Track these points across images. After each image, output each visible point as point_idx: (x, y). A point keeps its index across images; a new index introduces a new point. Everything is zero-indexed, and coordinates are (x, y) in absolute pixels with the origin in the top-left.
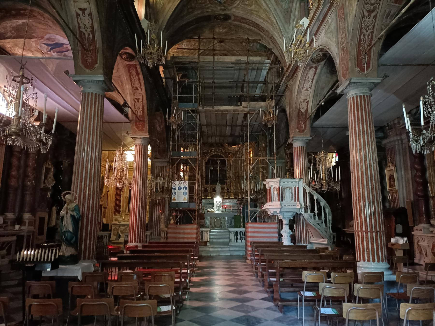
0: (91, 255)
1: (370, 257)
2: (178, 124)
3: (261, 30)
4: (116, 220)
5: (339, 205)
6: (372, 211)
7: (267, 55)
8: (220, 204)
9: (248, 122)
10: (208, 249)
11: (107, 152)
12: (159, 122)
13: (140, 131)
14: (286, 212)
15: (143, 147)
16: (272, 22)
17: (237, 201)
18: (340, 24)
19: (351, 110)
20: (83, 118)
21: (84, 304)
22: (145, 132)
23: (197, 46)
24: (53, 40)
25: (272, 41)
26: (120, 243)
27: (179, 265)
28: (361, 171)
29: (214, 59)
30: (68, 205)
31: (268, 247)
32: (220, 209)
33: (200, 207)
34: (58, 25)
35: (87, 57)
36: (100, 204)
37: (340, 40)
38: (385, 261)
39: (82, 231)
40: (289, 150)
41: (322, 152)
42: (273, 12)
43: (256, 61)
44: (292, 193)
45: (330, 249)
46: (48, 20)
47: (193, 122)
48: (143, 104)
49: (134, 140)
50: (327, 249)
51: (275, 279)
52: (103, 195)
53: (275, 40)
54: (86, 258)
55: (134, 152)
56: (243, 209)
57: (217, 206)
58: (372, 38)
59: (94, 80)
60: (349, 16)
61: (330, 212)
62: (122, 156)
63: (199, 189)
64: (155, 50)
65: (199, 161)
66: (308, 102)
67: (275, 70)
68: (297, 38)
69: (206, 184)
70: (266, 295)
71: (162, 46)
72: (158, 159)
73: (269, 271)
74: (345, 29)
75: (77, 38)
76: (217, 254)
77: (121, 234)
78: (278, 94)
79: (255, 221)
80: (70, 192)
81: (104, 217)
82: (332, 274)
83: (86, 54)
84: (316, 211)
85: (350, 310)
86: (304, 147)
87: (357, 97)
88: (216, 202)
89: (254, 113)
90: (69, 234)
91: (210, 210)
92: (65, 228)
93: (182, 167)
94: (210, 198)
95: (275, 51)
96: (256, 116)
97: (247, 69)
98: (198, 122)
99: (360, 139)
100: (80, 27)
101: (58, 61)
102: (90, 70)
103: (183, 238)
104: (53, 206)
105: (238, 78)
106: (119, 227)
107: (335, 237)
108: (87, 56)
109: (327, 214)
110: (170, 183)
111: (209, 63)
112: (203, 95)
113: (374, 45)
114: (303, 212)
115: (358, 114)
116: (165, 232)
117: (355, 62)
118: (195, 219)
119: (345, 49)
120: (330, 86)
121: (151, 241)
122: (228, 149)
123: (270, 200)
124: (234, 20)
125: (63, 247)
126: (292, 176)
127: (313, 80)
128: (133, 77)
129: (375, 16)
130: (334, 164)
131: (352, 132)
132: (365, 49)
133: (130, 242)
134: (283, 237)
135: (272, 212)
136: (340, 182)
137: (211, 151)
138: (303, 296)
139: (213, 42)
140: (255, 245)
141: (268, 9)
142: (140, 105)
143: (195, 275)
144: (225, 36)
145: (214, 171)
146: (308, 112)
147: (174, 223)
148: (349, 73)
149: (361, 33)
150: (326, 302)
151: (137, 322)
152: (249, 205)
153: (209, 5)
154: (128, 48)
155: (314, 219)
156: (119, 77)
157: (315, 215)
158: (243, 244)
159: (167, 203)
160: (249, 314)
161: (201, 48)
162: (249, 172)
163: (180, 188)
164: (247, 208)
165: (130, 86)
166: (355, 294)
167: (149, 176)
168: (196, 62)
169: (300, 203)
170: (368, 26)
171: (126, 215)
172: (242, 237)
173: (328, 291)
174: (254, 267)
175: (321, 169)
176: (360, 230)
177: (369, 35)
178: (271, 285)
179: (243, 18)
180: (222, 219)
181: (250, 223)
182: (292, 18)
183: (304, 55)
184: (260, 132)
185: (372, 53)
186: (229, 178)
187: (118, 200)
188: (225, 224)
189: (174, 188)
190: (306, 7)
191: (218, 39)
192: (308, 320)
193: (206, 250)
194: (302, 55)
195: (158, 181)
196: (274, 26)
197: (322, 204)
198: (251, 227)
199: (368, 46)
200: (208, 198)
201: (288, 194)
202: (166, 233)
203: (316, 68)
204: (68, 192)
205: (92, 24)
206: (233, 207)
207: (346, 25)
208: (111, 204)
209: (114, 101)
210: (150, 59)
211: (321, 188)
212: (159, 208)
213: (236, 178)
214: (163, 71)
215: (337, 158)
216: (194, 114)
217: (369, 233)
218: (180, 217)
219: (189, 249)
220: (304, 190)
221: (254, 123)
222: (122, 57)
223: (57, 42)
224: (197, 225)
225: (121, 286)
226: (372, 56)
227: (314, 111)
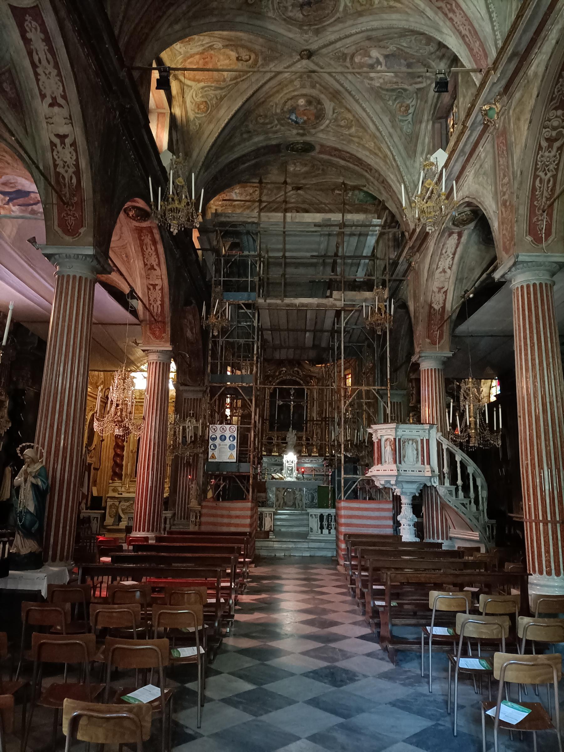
0: (65, 554)
1: (551, 566)
2: (223, 328)
3: (365, 168)
4: (114, 490)
5: (503, 472)
6: (555, 485)
7: (376, 212)
8: (294, 465)
9: (343, 325)
10: (271, 544)
11: (102, 373)
12: (190, 323)
13: (157, 339)
14: (408, 482)
16: (386, 156)
17: (323, 461)
18: (499, 161)
19: (518, 309)
20: (58, 318)
21: (44, 643)
22: (166, 342)
23: (256, 196)
24: (13, 184)
25: (384, 187)
26: (119, 531)
27: (215, 574)
28: (535, 415)
29: (285, 217)
30: (28, 466)
31: (374, 544)
32: (294, 474)
33: (259, 471)
34: (20, 162)
36: (88, 461)
37: (500, 188)
39: (50, 513)
40: (414, 374)
41: (470, 380)
42: (387, 139)
43: (358, 221)
44: (417, 450)
45: (483, 550)
46: (5, 154)
47: (248, 323)
48: (162, 293)
49: (146, 354)
50: (478, 549)
51: (383, 603)
52: (93, 446)
53: (390, 186)
54: (56, 558)
55: (146, 374)
56: (333, 476)
57: (288, 469)
59: (78, 255)
60: (515, 147)
61: (485, 485)
62: (124, 383)
63: (257, 439)
64: (183, 204)
65: (258, 390)
66: (446, 292)
67: (391, 236)
68: (426, 185)
69: (270, 430)
70: (367, 631)
71: (193, 197)
73: (374, 587)
74: (508, 168)
75: (50, 184)
76: (287, 553)
77: (122, 516)
78: (394, 277)
79: (354, 496)
80: (32, 444)
81: (95, 484)
82: (482, 597)
83: (66, 211)
84: (460, 482)
85: (506, 666)
86: (438, 369)
87: (528, 286)
88: (288, 462)
89: (352, 310)
90: (28, 516)
91: (276, 476)
92: (21, 506)
93: (228, 401)
94: (277, 454)
95: (390, 205)
96: (357, 314)
97: (341, 234)
98: (256, 324)
99: (533, 360)
100: (56, 166)
101: (20, 221)
102: (71, 237)
103: (229, 525)
104: (7, 466)
105: (327, 250)
106: (120, 502)
107: (495, 528)
109: (480, 488)
110: (206, 429)
111: (276, 224)
112: (266, 280)
113: (558, 197)
114: (437, 484)
115: (530, 316)
116: (196, 513)
117: (524, 226)
118: (248, 492)
119: (508, 204)
120: (484, 266)
121: (174, 529)
122: (310, 370)
123: (380, 461)
124: (320, 152)
125: (18, 539)
126: (418, 421)
127: (454, 254)
128: (147, 249)
130: (493, 399)
131: (520, 346)
132: (543, 204)
133: (136, 531)
134: (402, 526)
135: (383, 482)
136: (501, 433)
137: (280, 374)
138: (431, 636)
139: (283, 188)
140: (352, 539)
141: (378, 134)
142: (157, 294)
143: (246, 590)
144: (305, 178)
145: (284, 408)
146: (446, 310)
147: (213, 497)
148: (515, 245)
149: (536, 177)
150: (471, 646)
151: (137, 674)
152: (342, 469)
153: (278, 127)
154: (137, 199)
155: (457, 496)
156: (124, 247)
157: (457, 490)
158: (333, 537)
159: (201, 461)
160: (337, 664)
161: (264, 198)
162: (343, 411)
163: (223, 437)
164: (339, 475)
165: (141, 264)
166: (520, 635)
167: (172, 417)
168: (253, 223)
169: (431, 468)
170: (547, 166)
171: (131, 481)
172: (331, 525)
173: (471, 628)
174: (349, 578)
175: (469, 408)
176: (533, 518)
177: (549, 181)
178: (376, 612)
179: (336, 149)
180: (297, 492)
181: (343, 501)
182: (419, 148)
183: (437, 213)
184: (364, 342)
185: (555, 212)
186: (310, 421)
187: (118, 456)
188: (301, 500)
189: (214, 436)
190: (444, 132)
191: (293, 183)
192: (439, 678)
193: (268, 547)
194: (433, 214)
195: (187, 424)
196: (388, 161)
197: (470, 470)
198: (346, 508)
199: (547, 199)
200: (273, 454)
201: (410, 452)
202: (198, 515)
203: (460, 235)
204: (28, 444)
205: (77, 160)
206: (317, 471)
207: (510, 162)
208: (107, 464)
209: (114, 287)
210: (174, 220)
211: (468, 442)
212: (187, 470)
213: (322, 421)
214: (198, 237)
215: (499, 388)
216: (250, 311)
217: (550, 525)
218: (225, 486)
219: (236, 546)
220: (439, 444)
221: (354, 327)
222: (128, 215)
223: (20, 188)
224: (252, 502)
225: (110, 610)
226: (555, 216)
227: (456, 308)
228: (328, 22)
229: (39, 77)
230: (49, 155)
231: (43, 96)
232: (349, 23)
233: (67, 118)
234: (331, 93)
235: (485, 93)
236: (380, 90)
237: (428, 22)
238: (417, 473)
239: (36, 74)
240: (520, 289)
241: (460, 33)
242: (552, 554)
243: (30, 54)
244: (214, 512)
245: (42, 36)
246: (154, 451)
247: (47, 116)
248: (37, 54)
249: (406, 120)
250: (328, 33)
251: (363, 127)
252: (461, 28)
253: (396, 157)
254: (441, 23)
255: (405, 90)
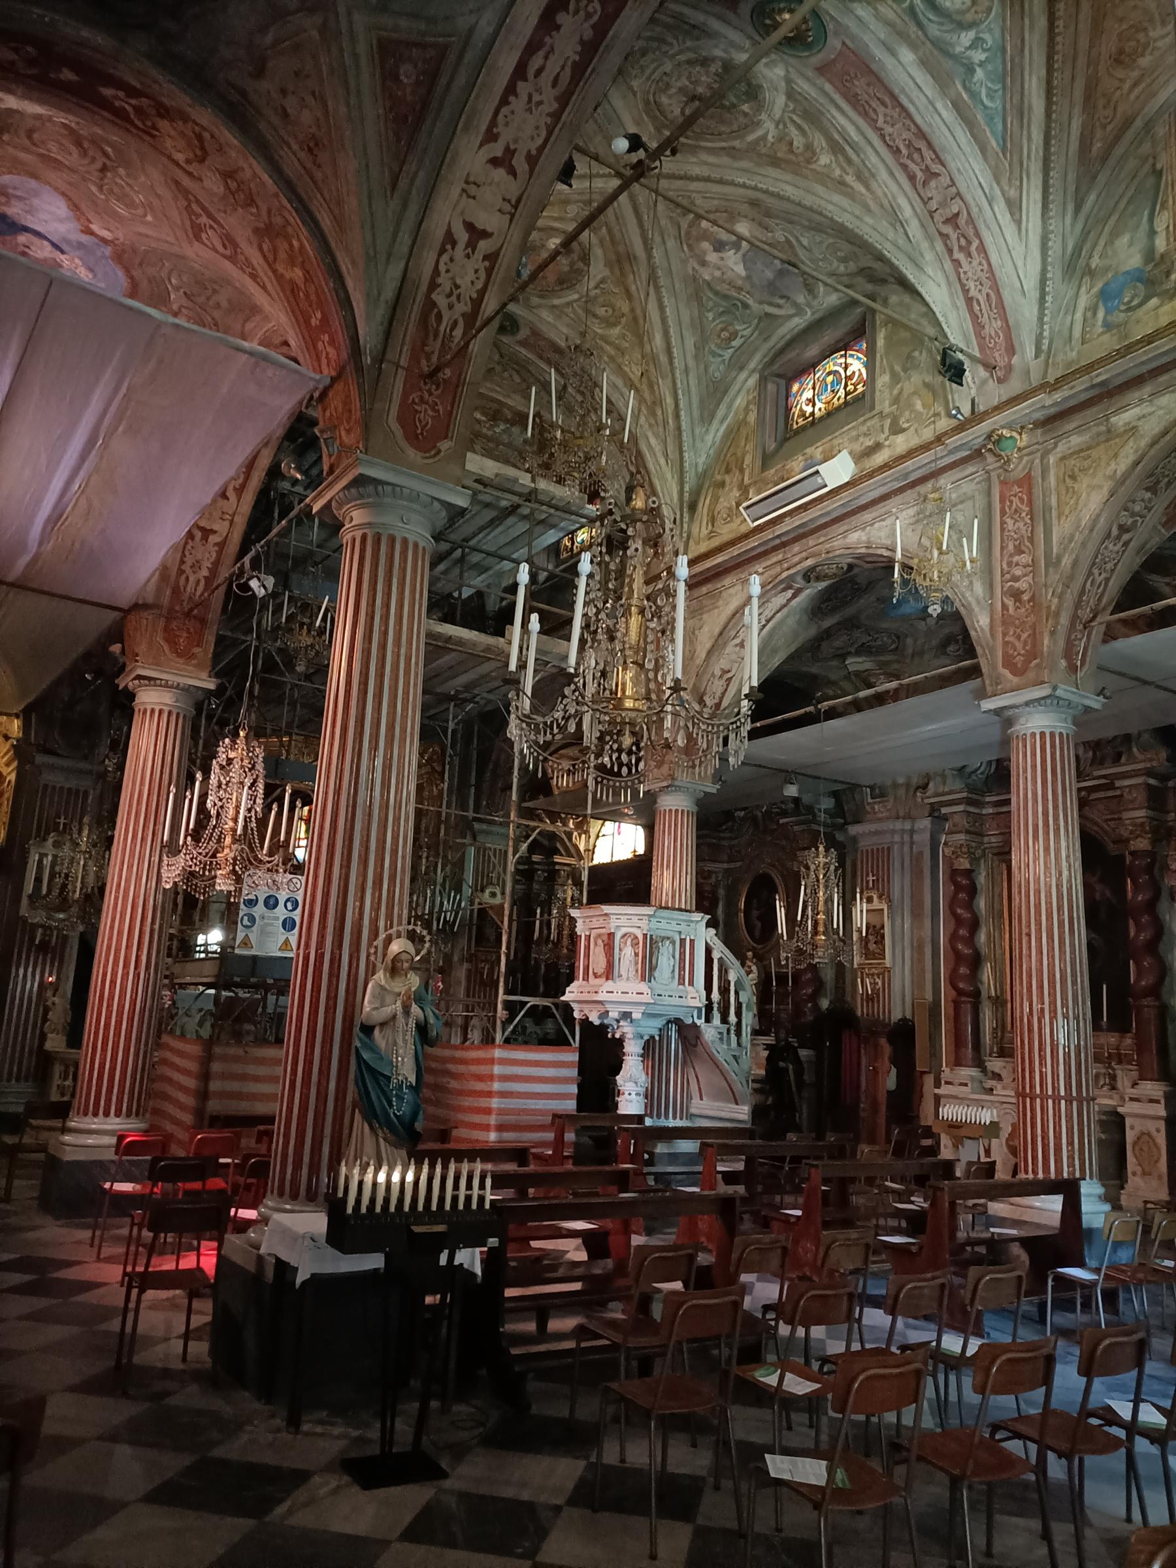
13: (179, 655)
15: (180, 721)
16: (658, 402)
22: (199, 666)
35: (422, 400)
38: (1091, 1178)
42: (678, 375)
48: (220, 553)
58: (1102, 594)
72: (58, 755)
83: (420, 390)
84: (732, 1018)
100: (433, 286)
108: (422, 398)
124: (523, 343)
129: (1126, 544)
141: (663, 359)
149: (1090, 573)
163: (272, 902)
181: (500, 1046)
196: (659, 413)
198: (503, 1062)
201: (666, 961)
202: (72, 1069)
205: (482, 293)
217: (1075, 1103)
220: (709, 951)
228: (709, 145)
229: (512, 99)
230: (429, 258)
231: (491, 136)
232: (744, 164)
233: (509, 201)
234: (617, 254)
235: (1015, 412)
236: (705, 287)
237: (901, 241)
238: (676, 1001)
239: (511, 90)
240: (1038, 737)
241: (966, 291)
242: (1076, 1146)
243: (532, 48)
244: (237, 1068)
245: (588, 34)
246: (153, 923)
247: (472, 179)
248: (546, 58)
249: (720, 356)
250: (694, 160)
251: (640, 335)
252: (971, 285)
253: (682, 413)
254: (929, 256)
255: (746, 306)
